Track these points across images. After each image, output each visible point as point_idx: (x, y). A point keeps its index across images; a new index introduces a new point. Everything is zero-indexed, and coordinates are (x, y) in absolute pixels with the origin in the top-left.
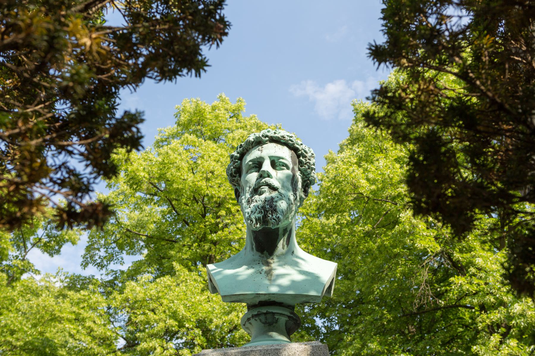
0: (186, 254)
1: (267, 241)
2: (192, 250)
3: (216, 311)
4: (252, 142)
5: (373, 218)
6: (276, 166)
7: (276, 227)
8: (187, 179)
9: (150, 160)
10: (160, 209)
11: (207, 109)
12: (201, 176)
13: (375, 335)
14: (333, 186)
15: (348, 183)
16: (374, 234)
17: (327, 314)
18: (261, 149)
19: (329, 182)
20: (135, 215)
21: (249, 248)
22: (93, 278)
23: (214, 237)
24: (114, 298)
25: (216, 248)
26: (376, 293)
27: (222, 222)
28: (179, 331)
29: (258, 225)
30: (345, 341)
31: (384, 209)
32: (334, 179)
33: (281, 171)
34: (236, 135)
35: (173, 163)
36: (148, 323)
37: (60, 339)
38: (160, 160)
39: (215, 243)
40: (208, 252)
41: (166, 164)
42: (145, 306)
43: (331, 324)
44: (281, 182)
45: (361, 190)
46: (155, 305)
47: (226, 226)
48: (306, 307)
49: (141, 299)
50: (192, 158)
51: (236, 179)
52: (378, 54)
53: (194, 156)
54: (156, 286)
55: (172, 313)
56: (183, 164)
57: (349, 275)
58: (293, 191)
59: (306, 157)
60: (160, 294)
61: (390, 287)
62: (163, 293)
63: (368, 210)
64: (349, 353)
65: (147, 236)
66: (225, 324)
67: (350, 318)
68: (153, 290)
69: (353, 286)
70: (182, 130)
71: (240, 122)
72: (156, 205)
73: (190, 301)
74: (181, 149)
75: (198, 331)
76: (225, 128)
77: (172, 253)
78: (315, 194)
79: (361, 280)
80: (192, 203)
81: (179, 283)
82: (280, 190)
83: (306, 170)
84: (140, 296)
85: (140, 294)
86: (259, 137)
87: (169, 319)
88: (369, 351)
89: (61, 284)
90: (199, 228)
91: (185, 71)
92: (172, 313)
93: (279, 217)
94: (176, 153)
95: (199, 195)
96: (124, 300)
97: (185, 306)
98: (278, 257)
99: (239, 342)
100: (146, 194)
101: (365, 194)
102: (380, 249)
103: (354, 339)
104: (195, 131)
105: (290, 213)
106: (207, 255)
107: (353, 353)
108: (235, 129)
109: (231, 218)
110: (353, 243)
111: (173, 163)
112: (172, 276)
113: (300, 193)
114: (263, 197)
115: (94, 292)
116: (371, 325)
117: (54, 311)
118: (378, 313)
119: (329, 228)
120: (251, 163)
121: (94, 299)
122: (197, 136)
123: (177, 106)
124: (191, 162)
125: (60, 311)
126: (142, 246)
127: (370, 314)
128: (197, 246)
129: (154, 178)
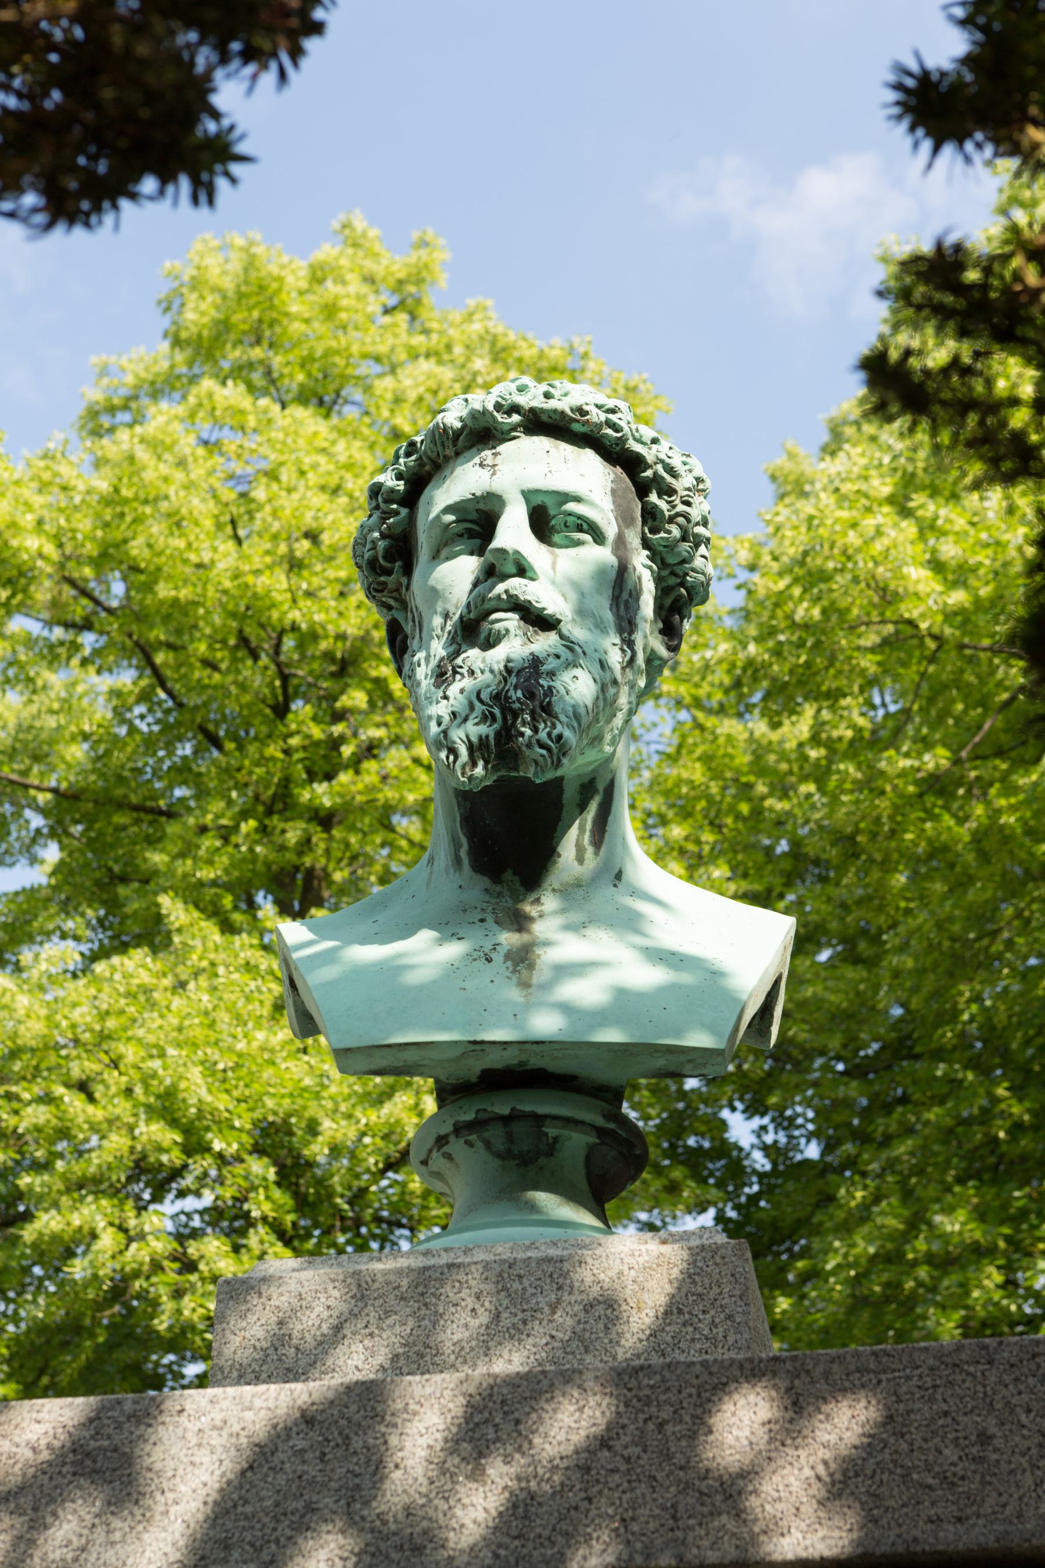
0: (210, 862)
1: (514, 829)
2: (237, 846)
3: (333, 1089)
4: (457, 434)
5: (958, 720)
6: (553, 530)
7: (550, 775)
8: (212, 564)
9: (65, 489)
10: (105, 683)
11: (290, 279)
12: (268, 552)
13: (961, 1181)
14: (797, 591)
15: (856, 580)
16: (959, 785)
17: (773, 1100)
18: (489, 461)
19: (781, 574)
20: (9, 708)
21: (443, 859)
23: (322, 794)
25: (331, 838)
26: (966, 1017)
27: (355, 735)
28: (185, 1166)
29: (479, 770)
31: (1000, 684)
32: (802, 563)
33: (572, 551)
34: (407, 382)
35: (156, 500)
36: (64, 1133)
38: (103, 486)
39: (325, 820)
40: (300, 854)
41: (126, 501)
42: (49, 1069)
43: (790, 1137)
44: (573, 596)
45: (910, 610)
46: (91, 1066)
47: (370, 750)
49: (33, 1043)
50: (231, 477)
51: (391, 580)
52: (935, 108)
53: (238, 468)
54: (93, 991)
55: (158, 1097)
56: (196, 501)
57: (862, 946)
58: (620, 630)
59: (671, 491)
60: (111, 1023)
61: (1022, 994)
62: (123, 1020)
63: (939, 689)
64: (857, 1250)
65: (55, 791)
66: (367, 1140)
67: (866, 1114)
68: (81, 1006)
69: (877, 987)
70: (190, 364)
71: (426, 332)
72: (92, 669)
73: (230, 1049)
74: (187, 443)
75: (261, 1168)
76: (365, 356)
77: (157, 858)
78: (729, 622)
79: (910, 963)
80: (234, 660)
81: (184, 977)
82: (566, 628)
83: (671, 546)
84: (32, 1031)
85: (30, 1024)
86: (485, 412)
87: (148, 1121)
88: (935, 1247)
90: (263, 760)
91: (149, 185)
92: (158, 1097)
93: (560, 737)
94: (167, 456)
95: (262, 626)
97: (209, 1067)
98: (565, 892)
99: (425, 1208)
100: (49, 624)
101: (924, 626)
102: (986, 845)
103: (877, 1199)
104: (241, 368)
105: (609, 721)
106: (297, 868)
107: (872, 1250)
108: (403, 357)
109: (390, 719)
110: (878, 820)
111: (156, 500)
112: (155, 950)
113: (648, 636)
114: (498, 655)
116: (945, 1142)
118: (975, 1094)
119: (783, 756)
120: (450, 518)
122: (251, 388)
123: (167, 265)
124: (228, 494)
126: (38, 831)
127: (942, 1102)
128: (257, 830)
129: (79, 561)
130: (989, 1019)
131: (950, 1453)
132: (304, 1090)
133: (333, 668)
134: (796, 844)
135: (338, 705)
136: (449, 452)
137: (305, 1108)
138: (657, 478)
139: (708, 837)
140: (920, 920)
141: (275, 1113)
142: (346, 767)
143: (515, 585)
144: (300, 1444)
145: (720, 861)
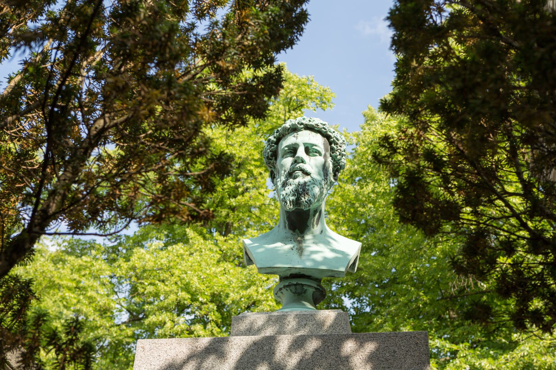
1: (298, 221)
3: (233, 285)
4: (289, 129)
6: (310, 152)
7: (308, 209)
12: (220, 133)
13: (409, 318)
19: (365, 146)
21: (282, 226)
22: (95, 243)
23: (233, 202)
24: (119, 266)
26: (412, 272)
27: (243, 186)
29: (292, 207)
30: (374, 324)
33: (314, 157)
37: (54, 309)
39: (233, 209)
40: (226, 218)
43: (362, 305)
47: (247, 190)
48: (334, 285)
49: (150, 269)
51: (272, 161)
54: (167, 255)
57: (384, 251)
59: (337, 144)
60: (172, 264)
62: (175, 263)
66: (243, 299)
67: (384, 298)
68: (164, 258)
69: (388, 262)
75: (213, 306)
79: (397, 257)
81: (192, 252)
84: (150, 265)
85: (150, 263)
86: (295, 124)
87: (182, 291)
89: (58, 248)
92: (184, 285)
93: (310, 200)
96: (130, 269)
97: (199, 277)
103: (385, 322)
106: (225, 222)
109: (253, 181)
110: (389, 216)
114: (296, 181)
115: (95, 258)
116: (405, 307)
117: (52, 277)
118: (414, 294)
119: (364, 196)
120: (286, 148)
121: (98, 266)
125: (60, 278)
130: (418, 273)
131: (388, 354)
132: (225, 285)
133: (237, 166)
134: (366, 221)
135: (238, 177)
136: (287, 133)
137: (225, 290)
138: (334, 141)
139: (342, 218)
140: (400, 244)
141: (217, 291)
142: (240, 195)
143: (301, 165)
144: (253, 348)
145: (345, 225)
